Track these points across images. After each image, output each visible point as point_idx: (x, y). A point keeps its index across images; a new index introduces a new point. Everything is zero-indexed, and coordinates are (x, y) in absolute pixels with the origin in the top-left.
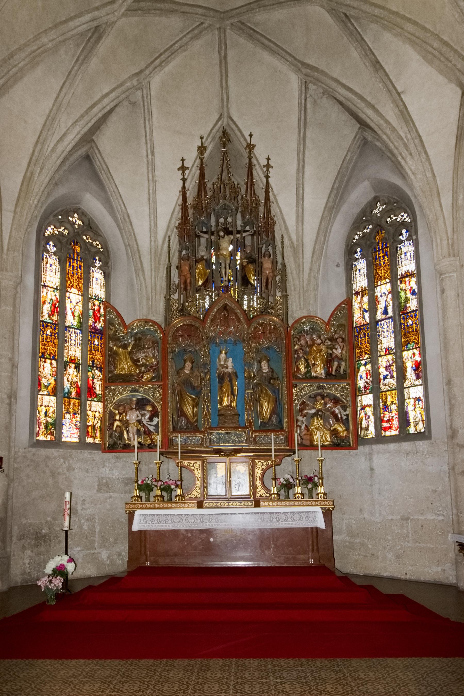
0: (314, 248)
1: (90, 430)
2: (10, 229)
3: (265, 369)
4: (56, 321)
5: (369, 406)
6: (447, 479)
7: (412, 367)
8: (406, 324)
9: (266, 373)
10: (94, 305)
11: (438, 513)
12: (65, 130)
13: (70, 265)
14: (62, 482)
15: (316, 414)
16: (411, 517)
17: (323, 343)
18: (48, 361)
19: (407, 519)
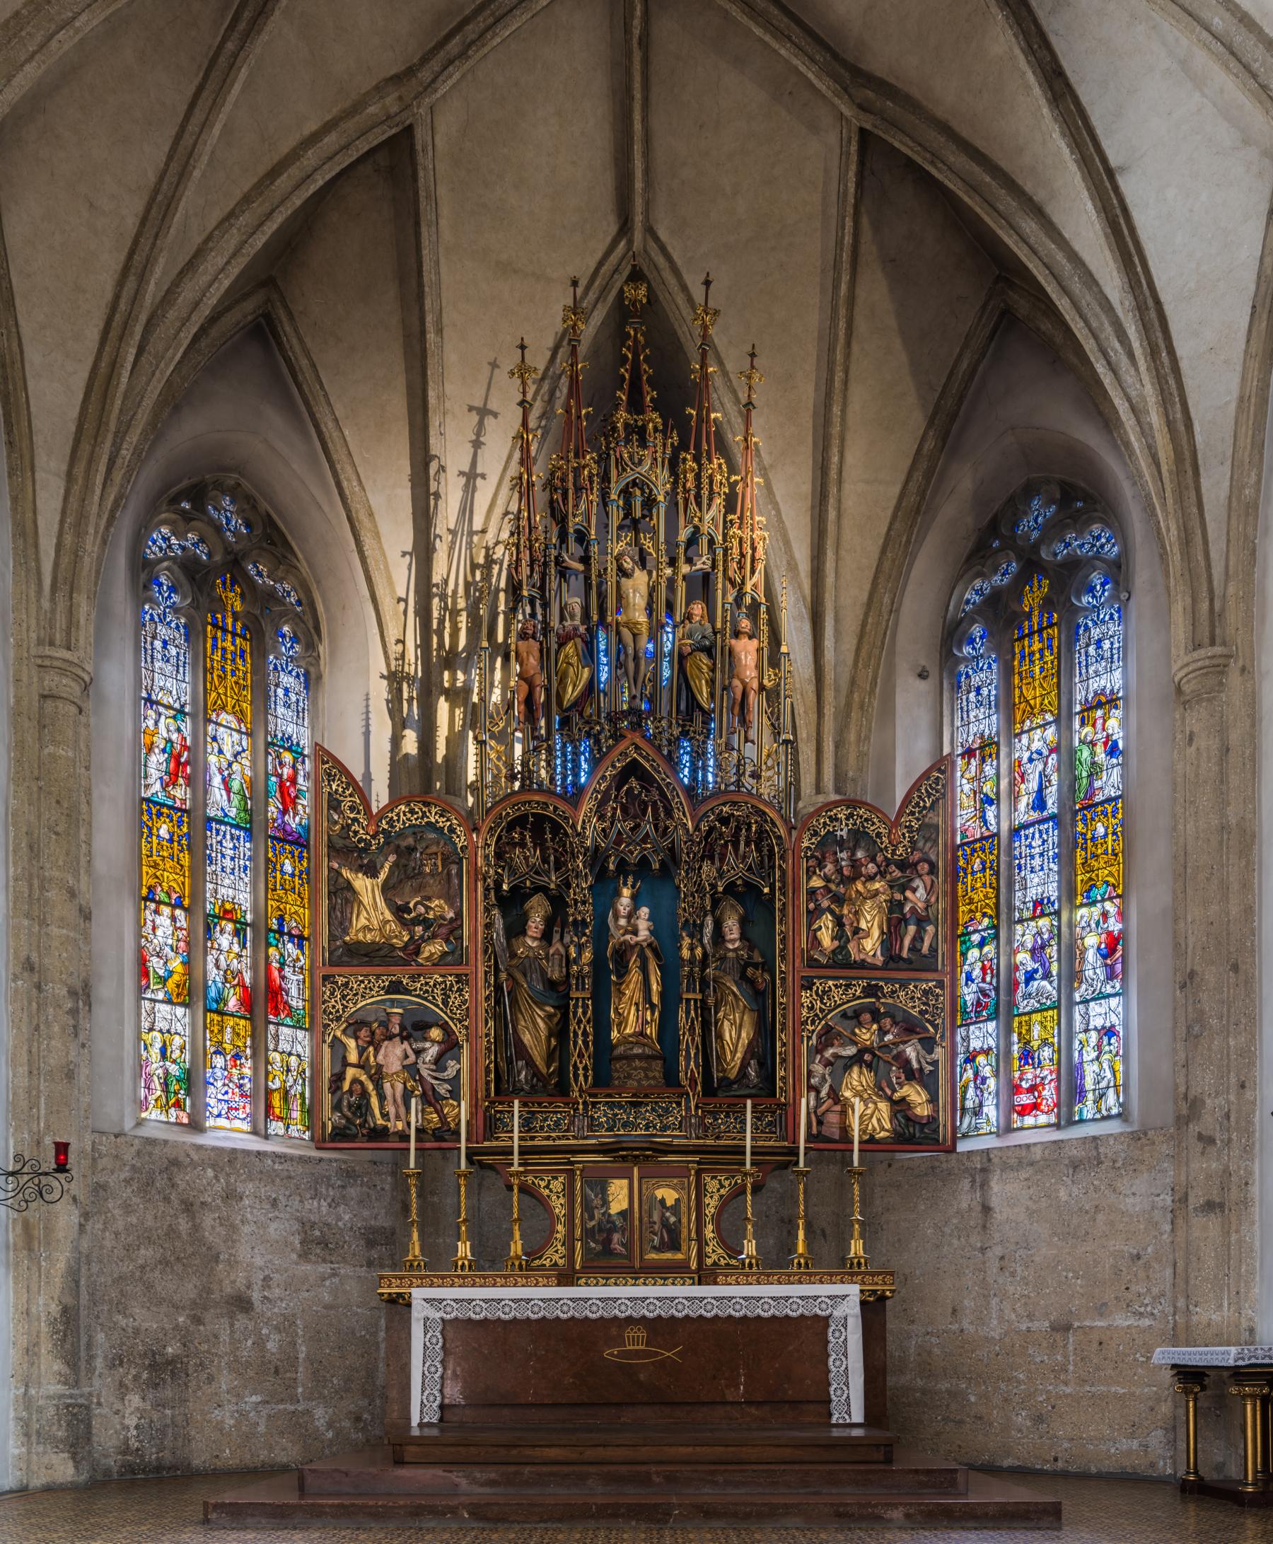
0: (864, 625)
1: (276, 1101)
2: (56, 527)
3: (733, 941)
4: (184, 801)
5: (986, 1052)
6: (1168, 1227)
7: (1099, 949)
8: (1089, 836)
9: (735, 950)
10: (281, 763)
11: (1142, 1310)
12: (198, 240)
13: (215, 646)
14: (213, 1227)
15: (857, 1059)
16: (1076, 1324)
17: (882, 874)
18: (166, 910)
19: (1068, 1328)
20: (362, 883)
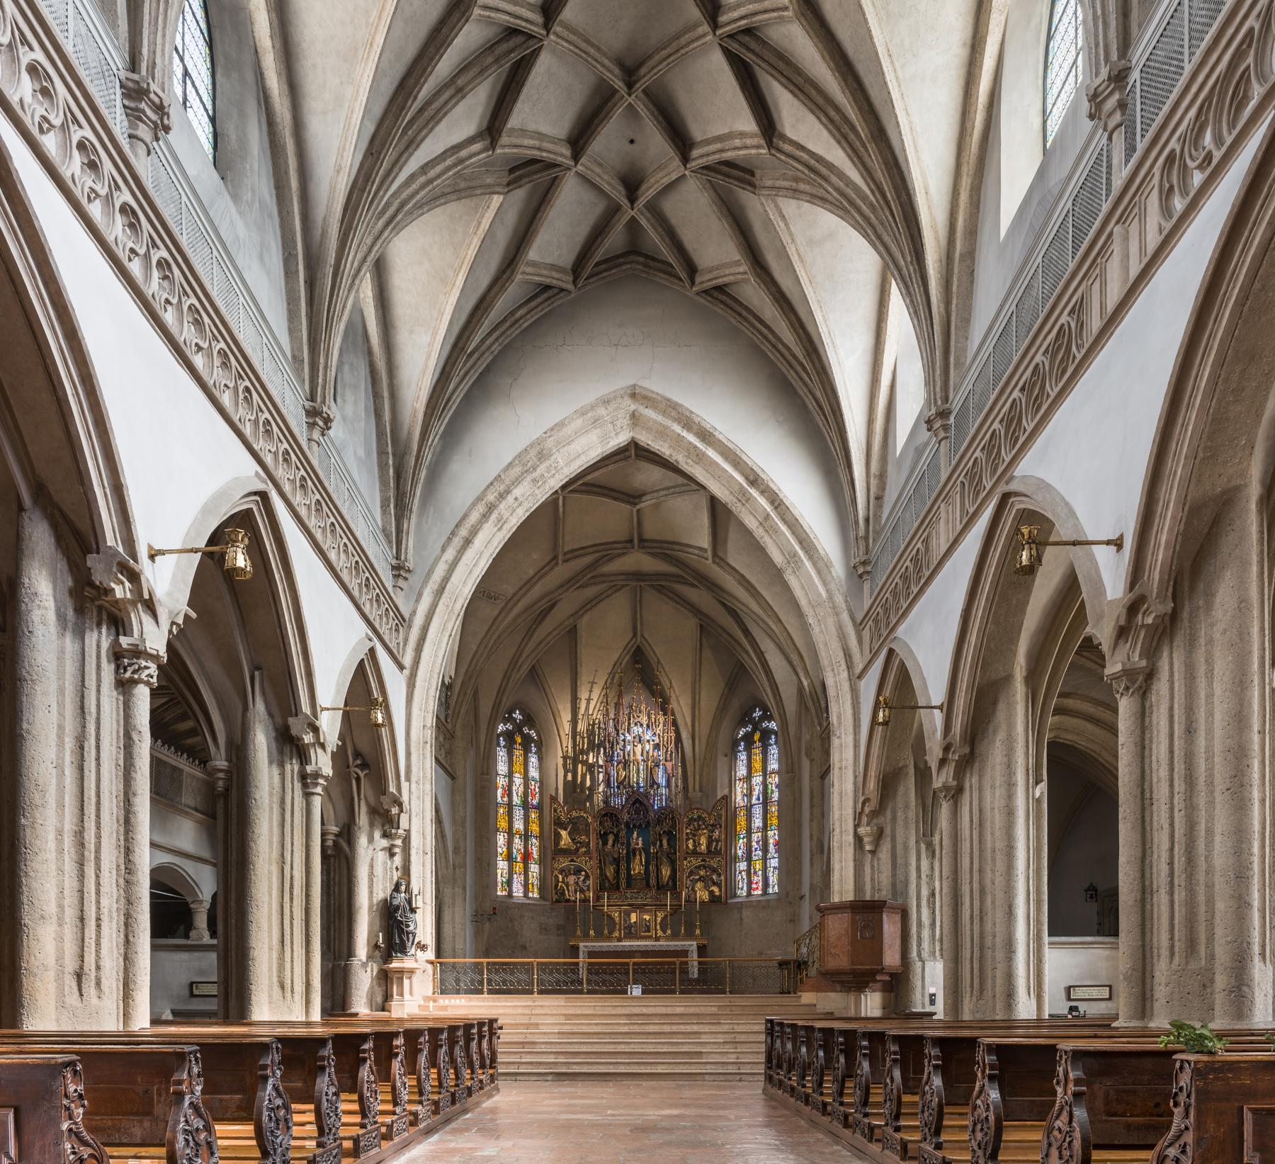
20: (564, 833)
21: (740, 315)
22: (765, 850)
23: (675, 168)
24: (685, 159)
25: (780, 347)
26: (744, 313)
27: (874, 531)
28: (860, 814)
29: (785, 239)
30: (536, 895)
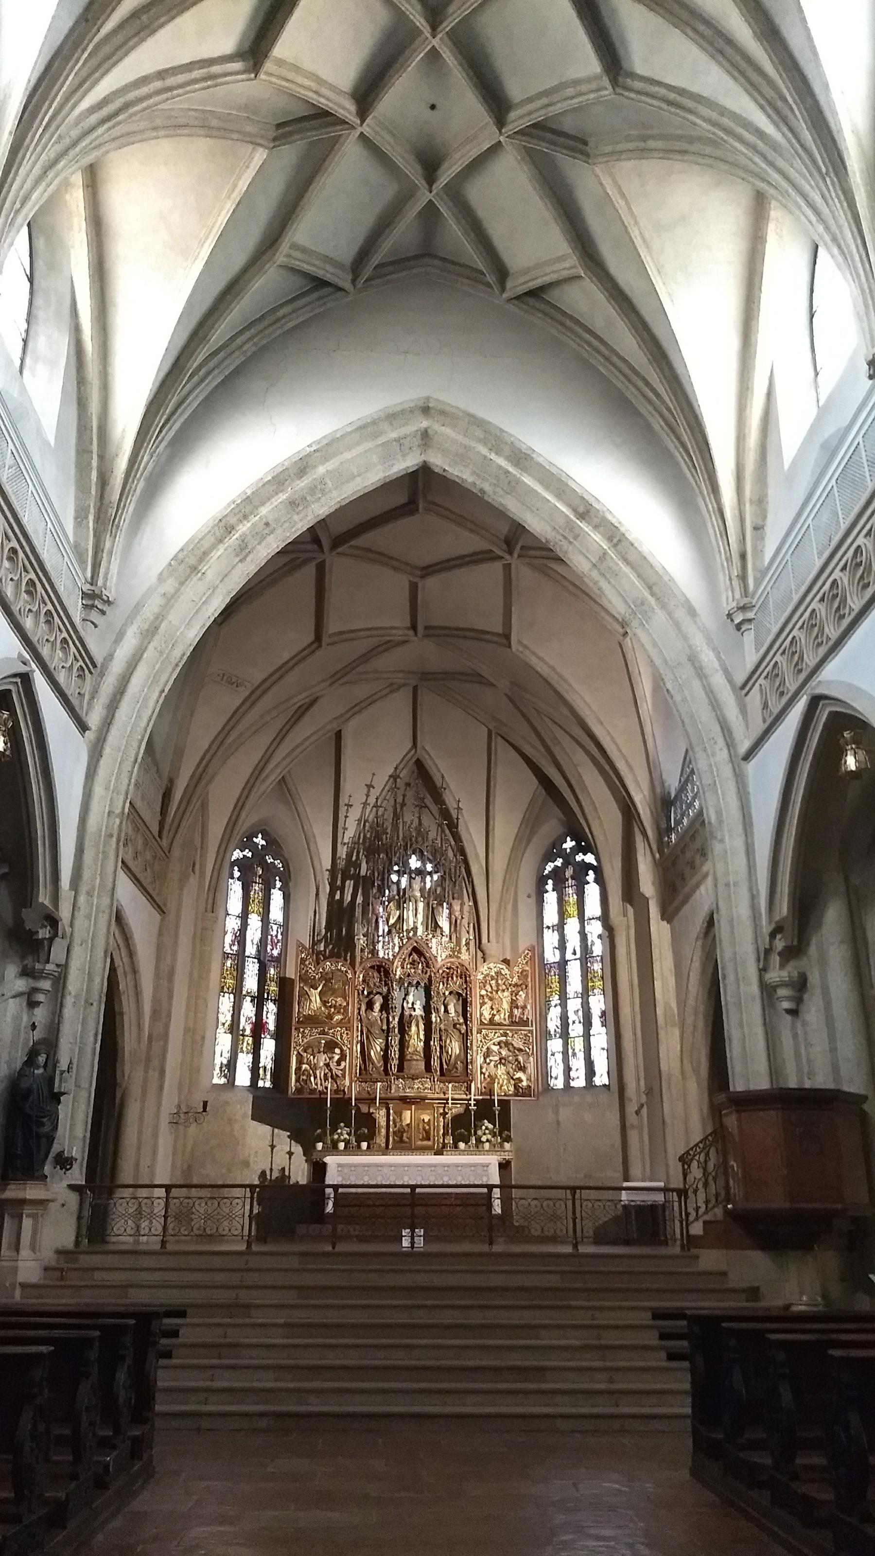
21: (563, 324)
22: (587, 1023)
23: (489, 135)
24: (500, 123)
25: (615, 359)
26: (568, 323)
27: (755, 569)
28: (768, 952)
29: (627, 219)
30: (268, 1084)
